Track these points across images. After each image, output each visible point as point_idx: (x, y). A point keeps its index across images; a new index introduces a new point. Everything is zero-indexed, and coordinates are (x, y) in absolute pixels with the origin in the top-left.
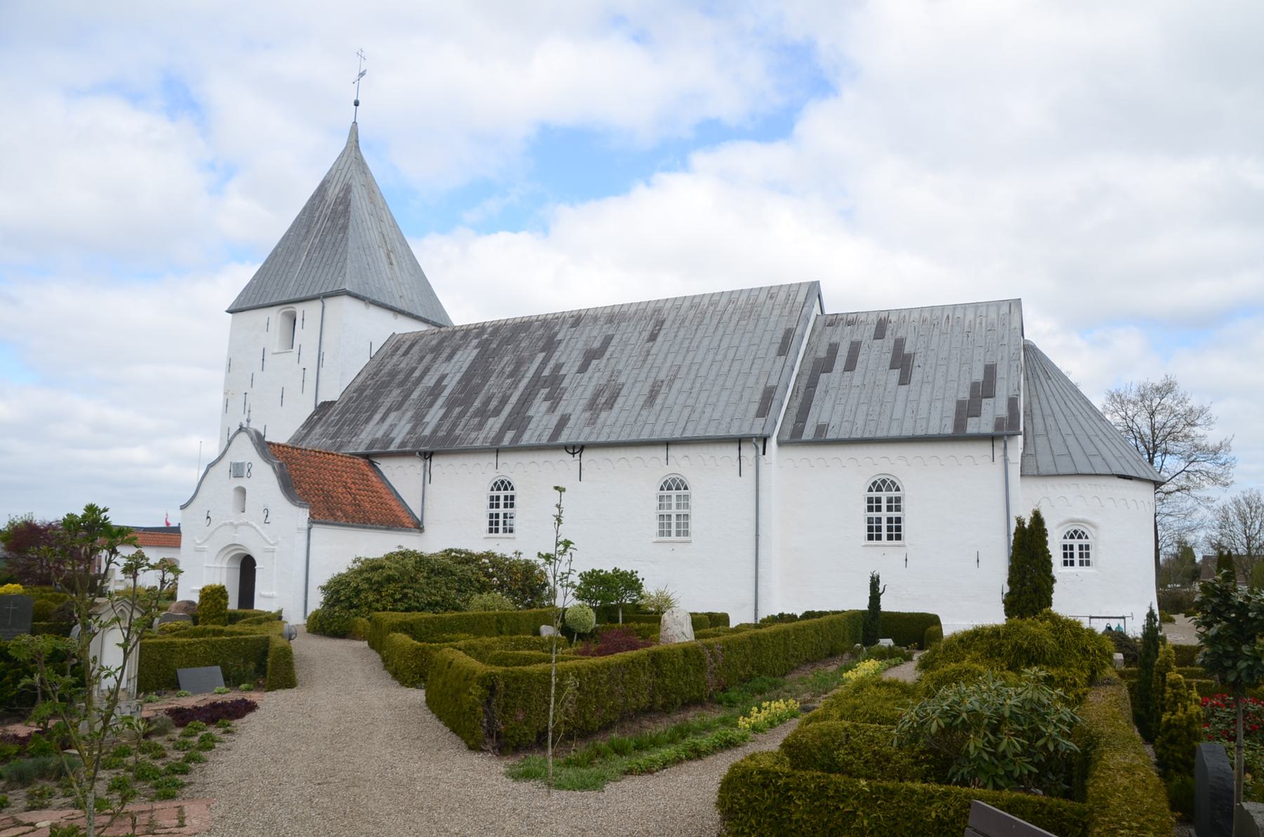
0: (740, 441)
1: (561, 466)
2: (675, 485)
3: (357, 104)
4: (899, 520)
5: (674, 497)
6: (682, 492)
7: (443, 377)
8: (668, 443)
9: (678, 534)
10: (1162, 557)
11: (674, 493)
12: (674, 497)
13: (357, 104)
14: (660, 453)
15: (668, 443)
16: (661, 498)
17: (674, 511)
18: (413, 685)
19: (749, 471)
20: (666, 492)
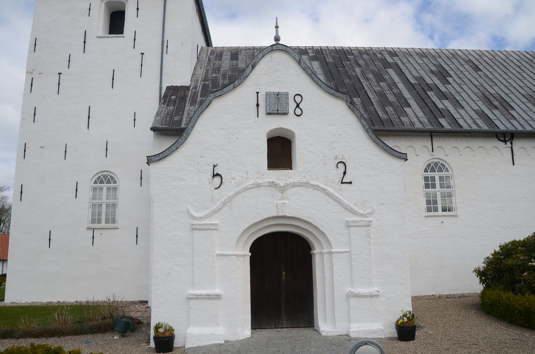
1: (495, 153)
6: (112, 185)
9: (107, 221)
11: (105, 186)
12: (105, 189)
16: (95, 189)
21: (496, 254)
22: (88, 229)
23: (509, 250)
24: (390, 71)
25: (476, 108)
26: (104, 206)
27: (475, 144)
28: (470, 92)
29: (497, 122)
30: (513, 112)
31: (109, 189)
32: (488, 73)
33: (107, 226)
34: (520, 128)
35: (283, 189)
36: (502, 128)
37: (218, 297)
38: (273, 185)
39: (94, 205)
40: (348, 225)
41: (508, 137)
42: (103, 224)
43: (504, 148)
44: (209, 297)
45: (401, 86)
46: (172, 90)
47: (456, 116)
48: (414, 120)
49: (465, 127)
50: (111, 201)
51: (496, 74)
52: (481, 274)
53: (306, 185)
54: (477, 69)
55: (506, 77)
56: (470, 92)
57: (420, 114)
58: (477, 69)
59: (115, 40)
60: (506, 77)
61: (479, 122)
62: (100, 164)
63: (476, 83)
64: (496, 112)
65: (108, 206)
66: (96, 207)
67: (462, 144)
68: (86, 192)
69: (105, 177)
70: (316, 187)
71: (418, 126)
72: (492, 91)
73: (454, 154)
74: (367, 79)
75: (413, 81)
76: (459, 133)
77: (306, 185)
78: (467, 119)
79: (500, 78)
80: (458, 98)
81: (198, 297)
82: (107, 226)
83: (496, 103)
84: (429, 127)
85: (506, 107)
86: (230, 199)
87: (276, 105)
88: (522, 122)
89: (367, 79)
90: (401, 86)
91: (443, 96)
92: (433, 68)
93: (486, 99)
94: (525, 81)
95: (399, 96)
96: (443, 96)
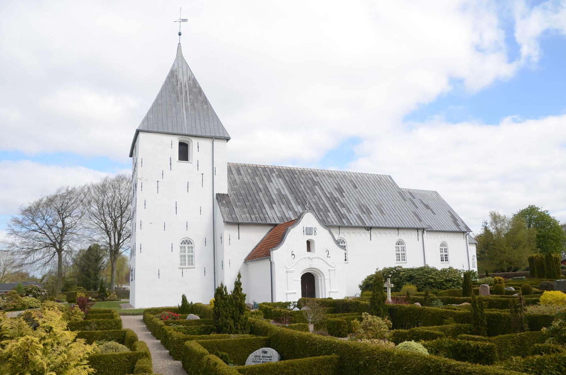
0: (417, 229)
1: (363, 235)
2: (443, 244)
3: (180, 34)
4: (192, 256)
5: (187, 247)
6: (190, 245)
7: (279, 190)
8: (398, 229)
9: (189, 265)
10: (6, 273)
11: (187, 246)
12: (187, 247)
13: (180, 34)
14: (396, 231)
15: (398, 229)
16: (181, 247)
17: (187, 254)
18: (159, 339)
19: (420, 239)
20: (183, 245)
21: (366, 279)
22: (179, 268)
23: (370, 278)
24: (316, 187)
25: (357, 213)
26: (187, 256)
27: (356, 231)
28: (353, 203)
29: (365, 221)
30: (371, 216)
31: (189, 247)
32: (360, 190)
33: (189, 266)
34: (374, 225)
35: (311, 259)
36: (368, 225)
37: (295, 293)
38: (309, 258)
39: (181, 256)
40: (329, 270)
41: (369, 229)
42: (187, 266)
43: (367, 233)
44: (293, 293)
45: (323, 198)
46: (218, 195)
47: (349, 218)
48: (333, 220)
49: (353, 224)
50: (191, 254)
51: (364, 191)
52: (360, 287)
53: (318, 258)
54: (355, 187)
55: (368, 193)
56: (353, 203)
57: (335, 217)
58: (355, 187)
59: (184, 164)
60: (368, 193)
61: (358, 221)
62: (184, 234)
63: (356, 197)
64: (365, 215)
65: (189, 256)
66: (182, 257)
67: (351, 231)
68: (177, 249)
69: (187, 241)
70: (321, 259)
71: (335, 223)
72: (363, 203)
73: (347, 236)
74: (308, 193)
75: (328, 195)
76: (351, 227)
77: (318, 258)
78: (354, 221)
79: (366, 194)
80: (349, 207)
81: (290, 293)
82: (189, 266)
83: (365, 210)
84: (339, 224)
85: (369, 212)
86: (297, 263)
87: (309, 231)
88: (375, 221)
89: (308, 193)
90: (323, 198)
91: (343, 206)
92: (336, 186)
93: (360, 207)
94: (375, 198)
95: (324, 205)
96: (343, 206)
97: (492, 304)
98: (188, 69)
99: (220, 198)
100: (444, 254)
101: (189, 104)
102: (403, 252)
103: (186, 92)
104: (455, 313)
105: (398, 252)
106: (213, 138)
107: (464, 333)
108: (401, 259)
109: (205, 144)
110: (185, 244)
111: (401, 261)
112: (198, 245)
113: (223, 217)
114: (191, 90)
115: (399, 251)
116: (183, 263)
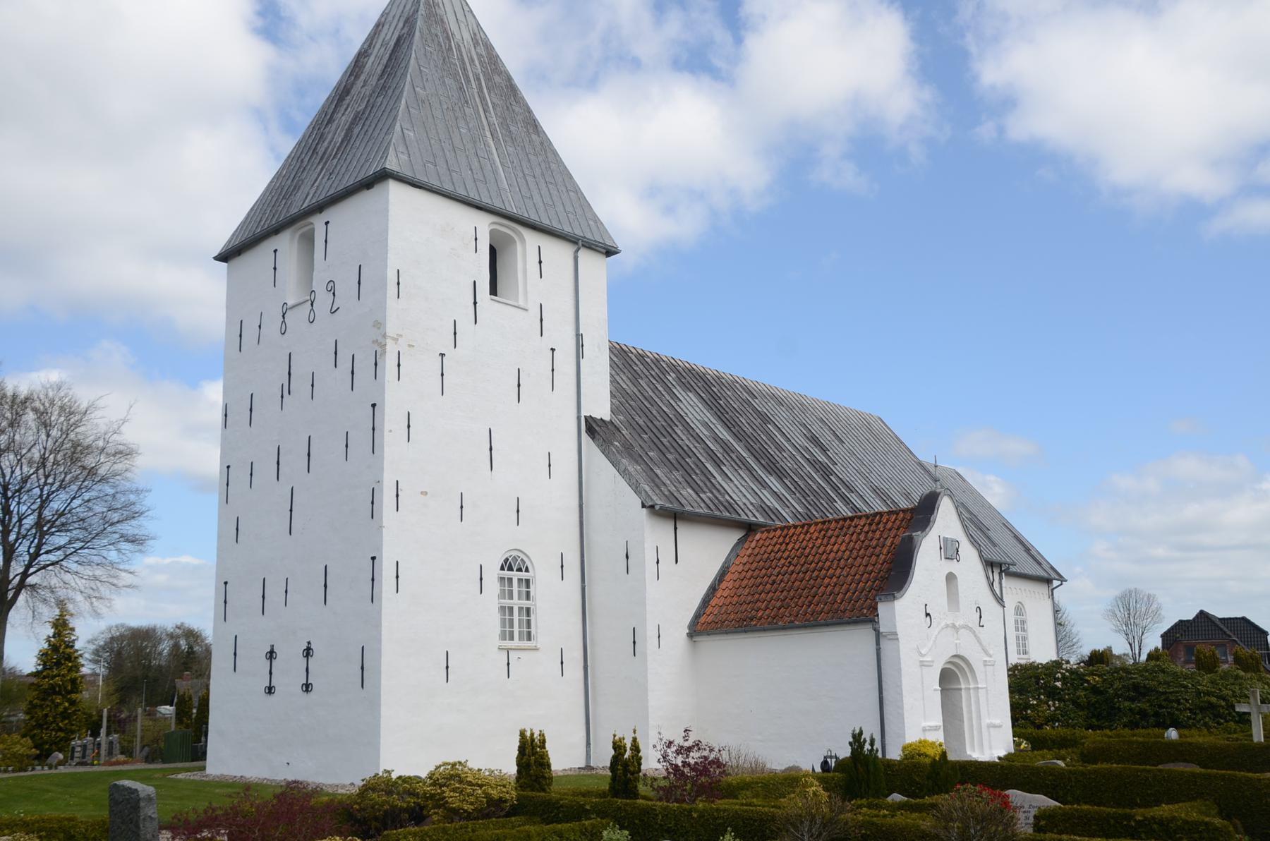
16: (502, 579)
39: (502, 608)
68: (492, 585)
97: (1208, 694)
98: (466, 8)
99: (593, 427)
100: (516, 603)
101: (494, 119)
102: (525, 603)
103: (479, 79)
104: (873, 824)
105: (507, 602)
106: (579, 242)
107: (1086, 803)
108: (516, 630)
109: (559, 254)
110: (510, 569)
111: (516, 642)
112: (543, 575)
113: (637, 489)
114: (489, 79)
115: (511, 597)
116: (507, 635)
